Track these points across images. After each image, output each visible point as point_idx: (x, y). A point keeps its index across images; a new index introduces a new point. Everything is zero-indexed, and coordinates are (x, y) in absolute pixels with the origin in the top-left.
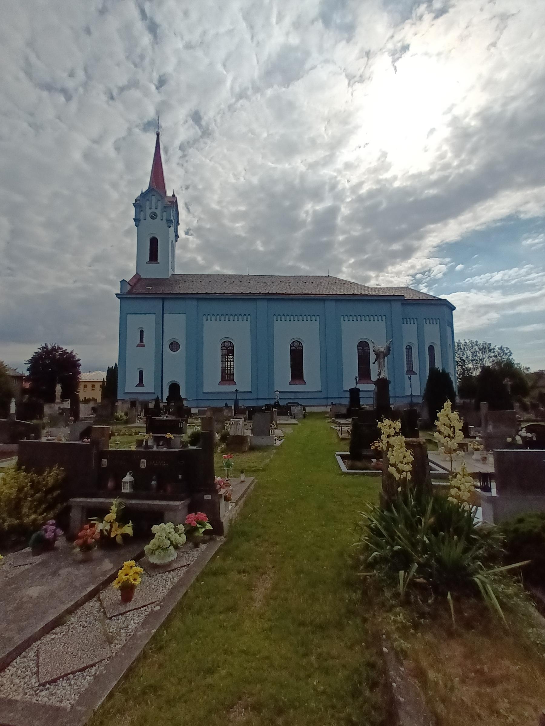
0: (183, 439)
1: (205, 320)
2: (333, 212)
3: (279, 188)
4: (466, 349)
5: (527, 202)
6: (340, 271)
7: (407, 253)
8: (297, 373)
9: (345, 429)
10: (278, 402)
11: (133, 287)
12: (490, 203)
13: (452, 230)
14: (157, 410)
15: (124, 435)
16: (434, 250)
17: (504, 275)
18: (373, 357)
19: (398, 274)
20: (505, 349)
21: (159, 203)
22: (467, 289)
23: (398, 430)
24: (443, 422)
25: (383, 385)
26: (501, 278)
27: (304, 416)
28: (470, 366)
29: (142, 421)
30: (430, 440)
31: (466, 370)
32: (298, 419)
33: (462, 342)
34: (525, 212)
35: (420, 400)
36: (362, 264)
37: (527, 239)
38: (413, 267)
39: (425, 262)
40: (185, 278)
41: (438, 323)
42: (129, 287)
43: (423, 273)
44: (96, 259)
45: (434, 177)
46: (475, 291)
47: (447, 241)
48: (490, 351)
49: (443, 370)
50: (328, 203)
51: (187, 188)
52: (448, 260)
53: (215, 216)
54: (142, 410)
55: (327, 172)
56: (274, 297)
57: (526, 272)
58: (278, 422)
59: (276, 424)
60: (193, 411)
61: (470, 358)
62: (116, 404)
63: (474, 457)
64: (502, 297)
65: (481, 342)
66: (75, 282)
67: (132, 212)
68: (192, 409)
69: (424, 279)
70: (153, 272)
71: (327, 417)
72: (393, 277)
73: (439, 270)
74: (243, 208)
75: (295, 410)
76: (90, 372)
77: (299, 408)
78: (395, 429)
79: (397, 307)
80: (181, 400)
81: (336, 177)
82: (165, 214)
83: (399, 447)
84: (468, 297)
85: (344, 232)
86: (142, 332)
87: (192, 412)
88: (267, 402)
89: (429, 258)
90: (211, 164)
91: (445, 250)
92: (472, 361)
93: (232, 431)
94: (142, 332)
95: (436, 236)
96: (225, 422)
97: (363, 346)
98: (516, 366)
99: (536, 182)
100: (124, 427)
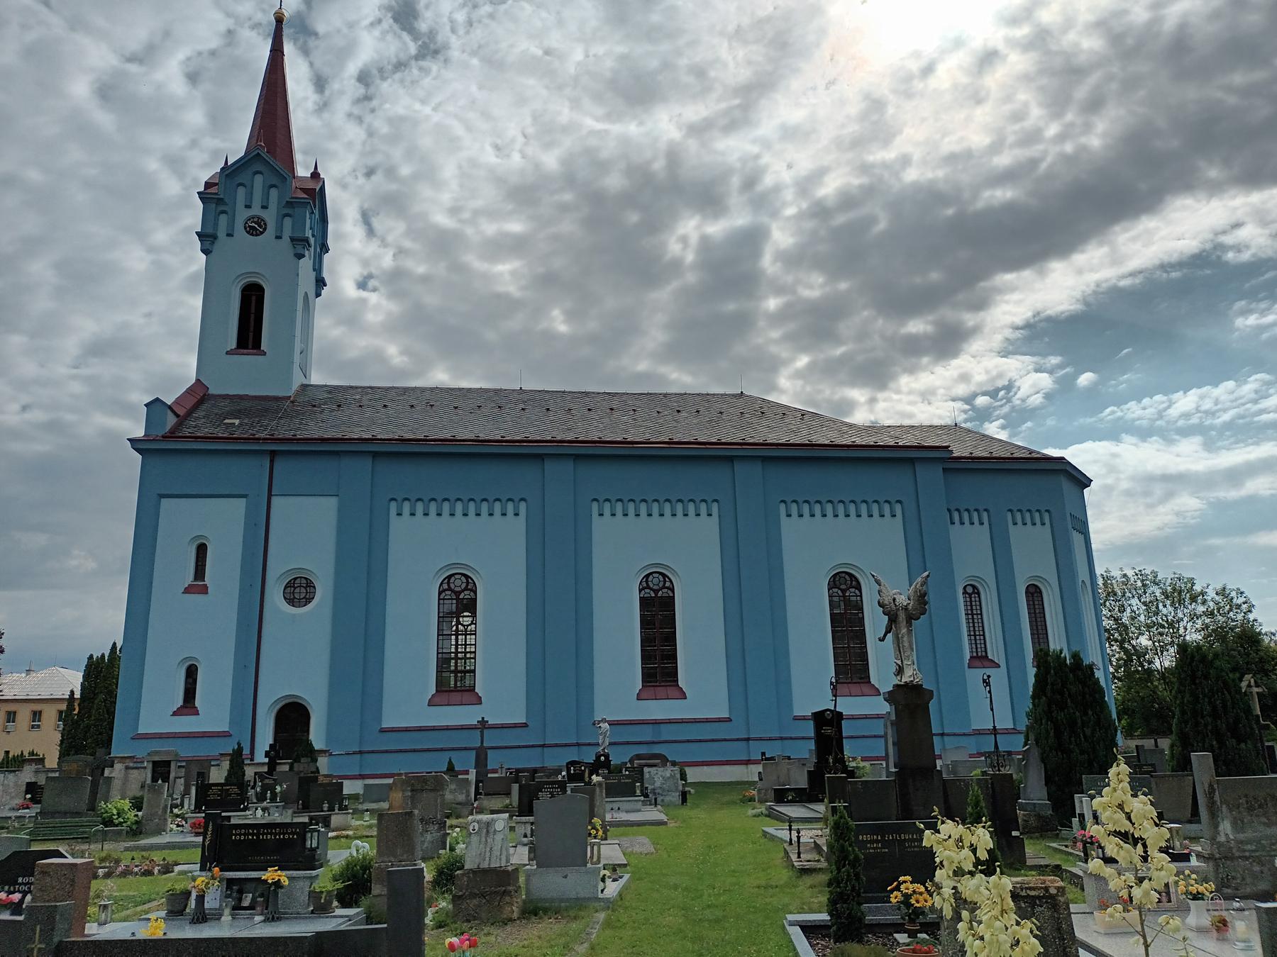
0: (317, 886)
1: (393, 511)
2: (752, 240)
3: (614, 182)
4: (1128, 594)
5: (1237, 225)
6: (773, 387)
7: (948, 342)
8: (660, 667)
9: (808, 835)
10: (607, 756)
11: (182, 420)
12: (1147, 223)
13: (1060, 285)
14: (235, 792)
15: (125, 873)
16: (1018, 334)
17: (1202, 397)
18: (874, 622)
19: (926, 396)
20: (1233, 594)
21: (274, 193)
22: (1113, 433)
23: (983, 855)
24: (1111, 827)
25: (911, 701)
26: (1194, 406)
27: (684, 796)
28: (1144, 641)
29: (187, 827)
30: (1058, 867)
31: (1133, 655)
32: (667, 806)
33: (1116, 573)
34: (1238, 248)
35: (1016, 744)
36: (828, 370)
37: (1245, 312)
38: (964, 378)
39: (996, 367)
40: (337, 397)
41: (1047, 521)
42: (171, 420)
43: (993, 394)
44: (97, 349)
45: (1004, 160)
46: (1133, 440)
47: (1049, 312)
48: (1194, 599)
49: (1076, 656)
50: (738, 219)
51: (370, 173)
52: (1054, 360)
53: (443, 244)
54: (186, 792)
55: (733, 148)
56: (591, 452)
57: (1256, 392)
58: (608, 817)
59: (604, 826)
60: (350, 788)
61: (1142, 618)
62: (107, 772)
63: (1192, 920)
64: (1205, 454)
65: (1165, 575)
66: (25, 408)
67: (194, 215)
68: (346, 783)
69: (995, 408)
70: (245, 377)
71: (752, 799)
72: (917, 401)
73: (1034, 385)
74: (516, 227)
75: (657, 777)
76: (28, 671)
77: (668, 771)
78: (974, 850)
79: (931, 476)
80: (312, 754)
81: (757, 157)
82: (288, 222)
83: (996, 912)
84: (1115, 455)
85: (779, 290)
86: (202, 550)
87: (345, 791)
88: (572, 755)
89: (1004, 353)
90: (436, 118)
91: (1041, 335)
92: (1148, 627)
93: (471, 853)
94: (202, 550)
95: (1019, 302)
96: (449, 822)
97: (844, 587)
98: (1267, 640)
99: (1253, 178)
100: (127, 849)
